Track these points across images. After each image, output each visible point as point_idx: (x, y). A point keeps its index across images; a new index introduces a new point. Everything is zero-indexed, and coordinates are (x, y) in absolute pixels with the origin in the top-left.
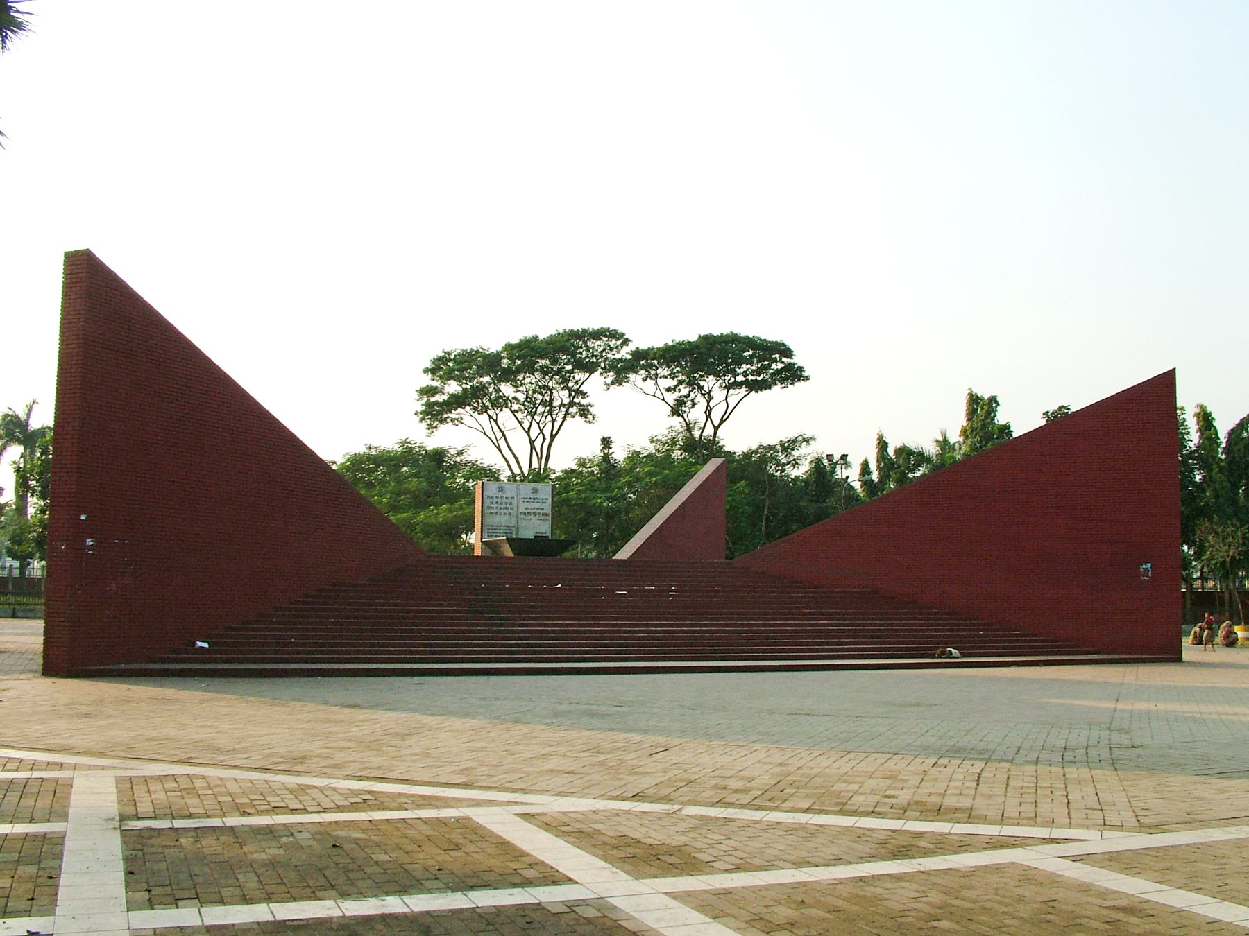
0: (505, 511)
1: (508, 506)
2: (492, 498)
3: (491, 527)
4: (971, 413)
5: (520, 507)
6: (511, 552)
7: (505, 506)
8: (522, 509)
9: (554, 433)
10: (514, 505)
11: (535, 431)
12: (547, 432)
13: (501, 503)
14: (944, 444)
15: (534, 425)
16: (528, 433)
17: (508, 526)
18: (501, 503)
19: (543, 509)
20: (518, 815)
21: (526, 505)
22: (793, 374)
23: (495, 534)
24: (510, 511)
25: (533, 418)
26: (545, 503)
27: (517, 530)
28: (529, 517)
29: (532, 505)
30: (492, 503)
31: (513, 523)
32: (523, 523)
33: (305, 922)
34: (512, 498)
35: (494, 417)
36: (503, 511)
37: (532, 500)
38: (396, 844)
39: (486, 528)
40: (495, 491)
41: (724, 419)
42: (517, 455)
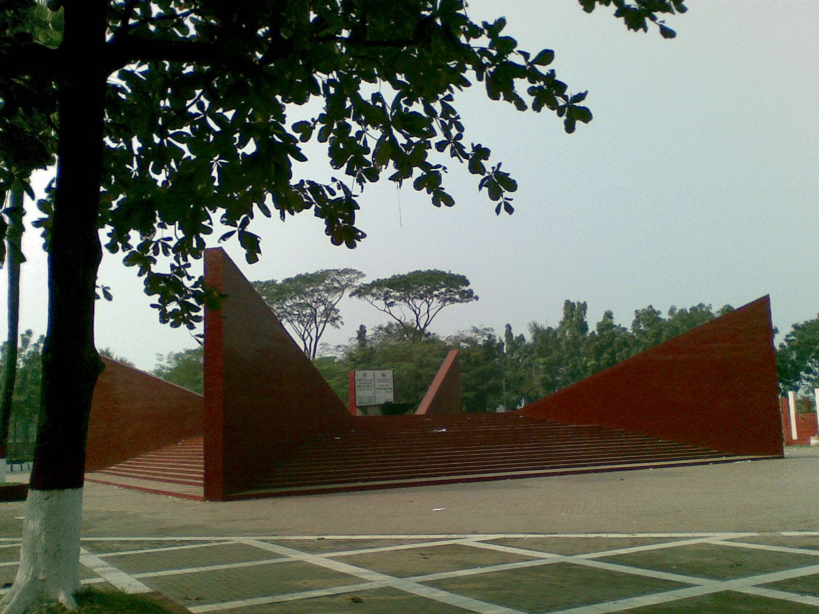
1: (370, 385)
2: (360, 380)
6: (419, 414)
12: (313, 334)
13: (365, 383)
20: (137, 579)
21: (379, 383)
22: (469, 296)
27: (375, 398)
29: (382, 384)
32: (378, 395)
33: (579, 567)
34: (372, 380)
41: (427, 323)
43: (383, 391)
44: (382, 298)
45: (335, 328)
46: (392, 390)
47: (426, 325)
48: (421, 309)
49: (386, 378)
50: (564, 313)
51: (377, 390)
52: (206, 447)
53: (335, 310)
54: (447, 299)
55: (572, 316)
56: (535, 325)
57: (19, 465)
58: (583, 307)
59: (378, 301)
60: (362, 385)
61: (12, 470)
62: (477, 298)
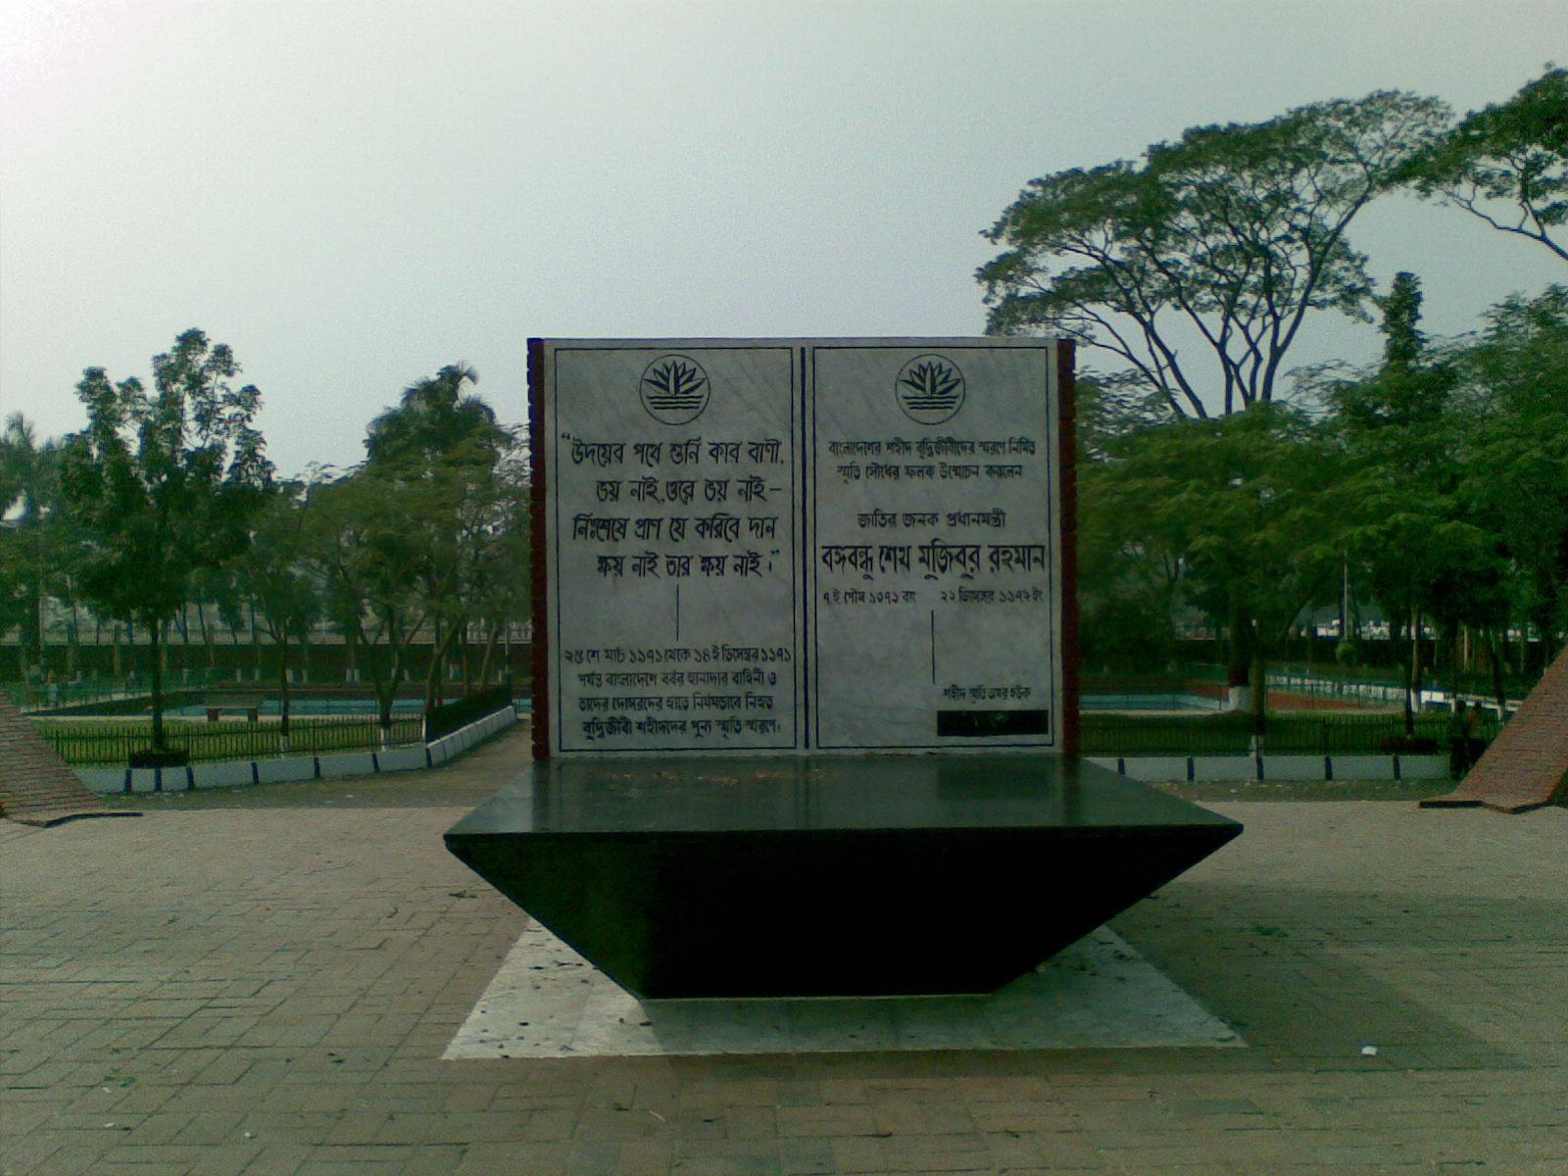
0: (716, 547)
1: (734, 506)
2: (609, 452)
3: (602, 666)
7: (708, 510)
8: (836, 525)
9: (1280, 342)
10: (779, 505)
11: (1237, 348)
13: (679, 490)
16: (1221, 346)
18: (679, 490)
19: (996, 518)
23: (636, 716)
24: (749, 540)
26: (1015, 471)
28: (889, 579)
29: (913, 494)
30: (609, 490)
31: (775, 631)
34: (761, 449)
36: (695, 545)
37: (913, 459)
38: (1048, 1080)
39: (572, 671)
42: (1200, 397)
43: (931, 589)
44: (1517, 188)
46: (1046, 576)
49: (958, 429)
51: (848, 577)
57: (150, 773)
61: (158, 786)
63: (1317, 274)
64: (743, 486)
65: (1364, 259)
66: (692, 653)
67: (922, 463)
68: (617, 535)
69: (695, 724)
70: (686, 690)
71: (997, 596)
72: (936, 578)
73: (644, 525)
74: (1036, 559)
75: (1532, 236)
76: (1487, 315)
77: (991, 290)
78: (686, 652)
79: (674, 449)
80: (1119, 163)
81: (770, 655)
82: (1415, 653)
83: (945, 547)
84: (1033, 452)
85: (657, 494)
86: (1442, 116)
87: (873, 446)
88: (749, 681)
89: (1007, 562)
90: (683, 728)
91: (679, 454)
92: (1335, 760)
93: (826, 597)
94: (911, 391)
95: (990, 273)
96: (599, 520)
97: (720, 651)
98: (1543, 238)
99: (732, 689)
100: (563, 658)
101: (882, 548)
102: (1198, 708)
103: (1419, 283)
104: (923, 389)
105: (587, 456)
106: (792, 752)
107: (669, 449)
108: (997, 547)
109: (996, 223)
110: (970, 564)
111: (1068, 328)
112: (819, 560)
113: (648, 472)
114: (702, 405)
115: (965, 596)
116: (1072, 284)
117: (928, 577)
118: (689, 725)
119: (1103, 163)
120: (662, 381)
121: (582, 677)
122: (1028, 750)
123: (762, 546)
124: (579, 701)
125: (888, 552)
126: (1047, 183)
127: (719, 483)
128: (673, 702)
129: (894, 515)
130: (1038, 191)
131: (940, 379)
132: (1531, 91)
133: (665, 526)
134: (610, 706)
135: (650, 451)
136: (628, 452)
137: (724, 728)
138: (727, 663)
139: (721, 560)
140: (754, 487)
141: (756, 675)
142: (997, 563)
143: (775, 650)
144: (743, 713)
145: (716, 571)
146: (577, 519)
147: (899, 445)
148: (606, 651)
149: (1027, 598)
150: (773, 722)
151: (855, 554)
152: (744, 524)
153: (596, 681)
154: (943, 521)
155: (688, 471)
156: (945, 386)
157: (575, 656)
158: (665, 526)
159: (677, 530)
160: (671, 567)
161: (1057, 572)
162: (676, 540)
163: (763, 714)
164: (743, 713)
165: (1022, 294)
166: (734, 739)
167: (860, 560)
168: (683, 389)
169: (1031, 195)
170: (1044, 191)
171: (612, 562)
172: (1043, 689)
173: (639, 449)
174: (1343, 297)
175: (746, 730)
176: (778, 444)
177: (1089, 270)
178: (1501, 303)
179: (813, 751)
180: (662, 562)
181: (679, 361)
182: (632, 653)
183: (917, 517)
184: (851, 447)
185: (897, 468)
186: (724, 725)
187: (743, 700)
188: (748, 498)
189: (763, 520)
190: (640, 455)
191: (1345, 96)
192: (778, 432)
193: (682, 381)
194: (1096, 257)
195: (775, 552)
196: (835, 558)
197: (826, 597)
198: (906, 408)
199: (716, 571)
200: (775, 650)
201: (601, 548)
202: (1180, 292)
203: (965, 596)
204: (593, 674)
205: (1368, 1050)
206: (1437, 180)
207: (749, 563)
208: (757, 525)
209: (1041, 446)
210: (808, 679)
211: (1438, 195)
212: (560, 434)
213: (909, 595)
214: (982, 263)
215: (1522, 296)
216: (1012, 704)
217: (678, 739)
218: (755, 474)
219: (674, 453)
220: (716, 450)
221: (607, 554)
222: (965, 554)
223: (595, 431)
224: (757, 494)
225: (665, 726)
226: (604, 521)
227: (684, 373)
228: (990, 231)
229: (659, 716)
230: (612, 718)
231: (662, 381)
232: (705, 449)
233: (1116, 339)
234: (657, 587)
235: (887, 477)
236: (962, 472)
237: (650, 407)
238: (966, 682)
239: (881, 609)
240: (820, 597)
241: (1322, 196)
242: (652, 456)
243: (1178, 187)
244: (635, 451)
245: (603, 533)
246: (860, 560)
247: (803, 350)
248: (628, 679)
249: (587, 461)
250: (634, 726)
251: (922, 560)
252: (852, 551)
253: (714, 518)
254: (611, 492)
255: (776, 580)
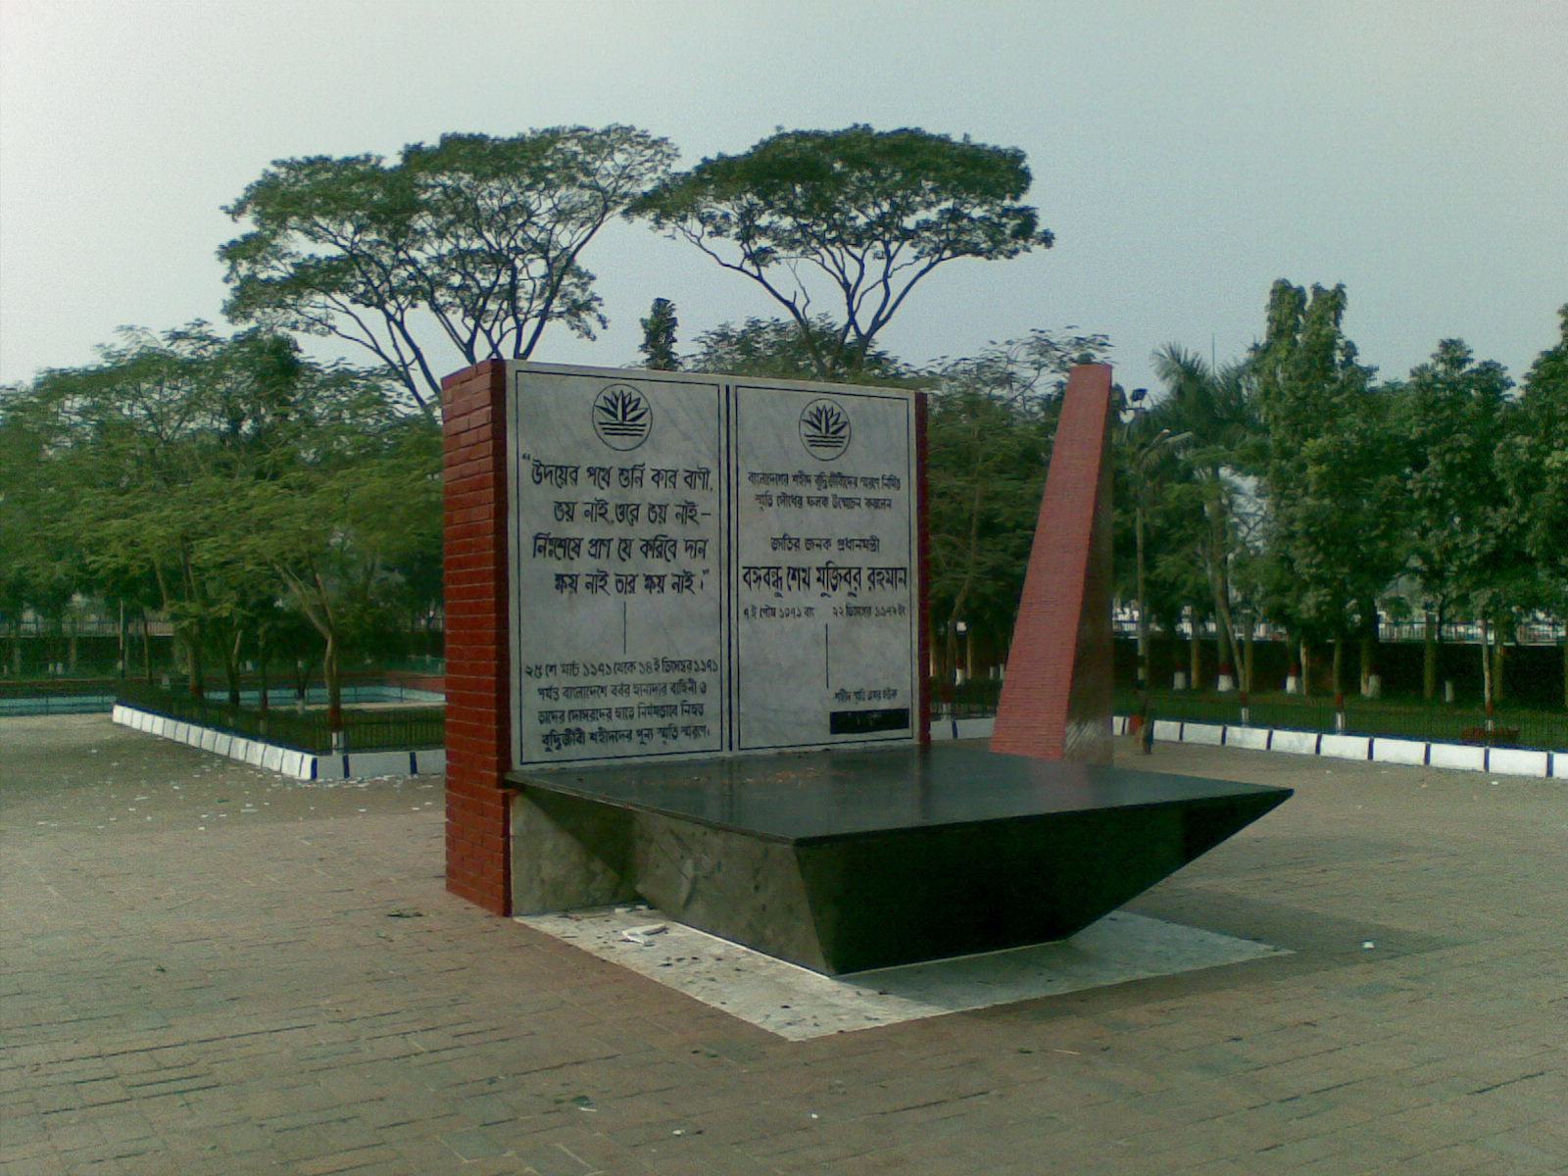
0: (657, 566)
1: (672, 529)
2: (564, 474)
3: (561, 681)
4: (1280, 330)
5: (746, 535)
8: (754, 551)
10: (708, 528)
13: (628, 512)
14: (1369, 372)
15: (481, 336)
17: (676, 665)
18: (628, 512)
19: (872, 544)
23: (589, 727)
24: (684, 560)
25: (477, 325)
28: (795, 597)
30: (565, 510)
31: (699, 643)
32: (760, 640)
34: (695, 476)
35: (398, 317)
36: (641, 564)
39: (533, 685)
40: (588, 432)
41: (881, 318)
43: (823, 604)
45: (580, 337)
46: (907, 594)
47: (877, 324)
48: (865, 262)
50: (1270, 319)
51: (755, 596)
52: (122, 704)
53: (579, 274)
54: (952, 240)
55: (1296, 328)
56: (1175, 355)
58: (1333, 301)
59: (718, 238)
60: (582, 530)
62: (1047, 239)
63: (551, 287)
64: (680, 510)
65: (592, 278)
66: (637, 665)
67: (819, 494)
68: (572, 554)
69: (639, 733)
70: (632, 701)
71: (874, 611)
72: (829, 596)
73: (595, 545)
74: (901, 579)
75: (752, 276)
76: (698, 340)
77: (233, 269)
78: (632, 664)
79: (621, 474)
80: (368, 157)
81: (701, 666)
82: (969, 650)
83: (836, 569)
84: (899, 488)
85: (608, 516)
86: (668, 156)
87: (782, 478)
88: (684, 691)
89: (880, 582)
90: (629, 736)
91: (626, 479)
92: (419, 754)
93: (746, 612)
94: (811, 431)
95: (232, 252)
96: (557, 539)
97: (660, 663)
98: (759, 278)
99: (671, 699)
100: (524, 675)
101: (789, 568)
102: (401, 699)
103: (674, 310)
104: (820, 429)
105: (546, 476)
106: (719, 754)
107: (618, 472)
108: (874, 569)
109: (237, 200)
110: (854, 584)
111: (311, 315)
112: (741, 578)
113: (601, 495)
114: (645, 433)
115: (852, 611)
116: (312, 271)
117: (823, 595)
118: (634, 734)
119: (352, 154)
120: (612, 409)
121: (541, 691)
122: (895, 744)
123: (696, 566)
124: (537, 715)
125: (794, 572)
126: (292, 166)
127: (660, 506)
128: (624, 713)
129: (798, 540)
130: (282, 172)
131: (831, 422)
132: (765, 147)
133: (614, 545)
134: (566, 719)
135: (602, 474)
136: (583, 473)
137: (663, 735)
138: (666, 674)
139: (661, 578)
140: (688, 511)
141: (689, 685)
142: (873, 583)
143: (706, 661)
144: (681, 720)
145: (657, 589)
146: (536, 538)
147: (802, 477)
148: (562, 665)
149: (895, 611)
150: (703, 728)
151: (768, 574)
152: (681, 546)
153: (554, 695)
154: (835, 546)
155: (634, 495)
156: (835, 427)
157: (535, 671)
158: (614, 545)
159: (624, 550)
160: (620, 585)
161: (915, 591)
162: (624, 560)
163: (697, 721)
164: (681, 720)
165: (263, 276)
166: (673, 745)
167: (772, 580)
168: (629, 417)
169: (274, 176)
170: (288, 173)
171: (568, 580)
172: (906, 694)
173: (591, 471)
174: (569, 310)
175: (589, 743)
176: (708, 472)
177: (330, 259)
178: (711, 330)
179: (736, 752)
180: (612, 580)
181: (626, 391)
182: (585, 666)
183: (816, 542)
184: (767, 478)
185: (801, 498)
186: (663, 731)
187: (679, 709)
188: (684, 522)
189: (696, 542)
190: (592, 478)
191: (589, 126)
192: (707, 462)
193: (628, 410)
194: (343, 247)
195: (706, 572)
196: (753, 577)
197: (746, 612)
198: (807, 444)
199: (657, 589)
200: (706, 661)
201: (560, 567)
202: (423, 289)
203: (852, 611)
204: (550, 689)
205: (1368, 945)
206: (668, 216)
207: (684, 581)
208: (691, 547)
209: (904, 482)
210: (732, 687)
211: (670, 225)
212: (520, 456)
213: (809, 611)
214: (225, 242)
215: (732, 327)
216: (884, 704)
217: (629, 747)
218: (689, 500)
219: (622, 478)
220: (657, 476)
221: (563, 573)
222: (849, 575)
223: (552, 455)
224: (691, 518)
225: (615, 736)
226: (561, 540)
227: (630, 402)
228: (231, 207)
229: (608, 726)
230: (567, 730)
231: (612, 409)
232: (649, 474)
233: (366, 335)
234: (608, 603)
235: (793, 505)
236: (849, 503)
237: (601, 433)
238: (851, 686)
239: (789, 623)
240: (741, 612)
241: (561, 215)
242: (603, 479)
243: (426, 188)
244: (587, 474)
245: (560, 551)
246: (772, 580)
247: (727, 388)
248: (581, 691)
249: (546, 482)
250: (587, 736)
251: (819, 580)
252: (766, 571)
253: (656, 540)
254: (567, 513)
255: (705, 598)
